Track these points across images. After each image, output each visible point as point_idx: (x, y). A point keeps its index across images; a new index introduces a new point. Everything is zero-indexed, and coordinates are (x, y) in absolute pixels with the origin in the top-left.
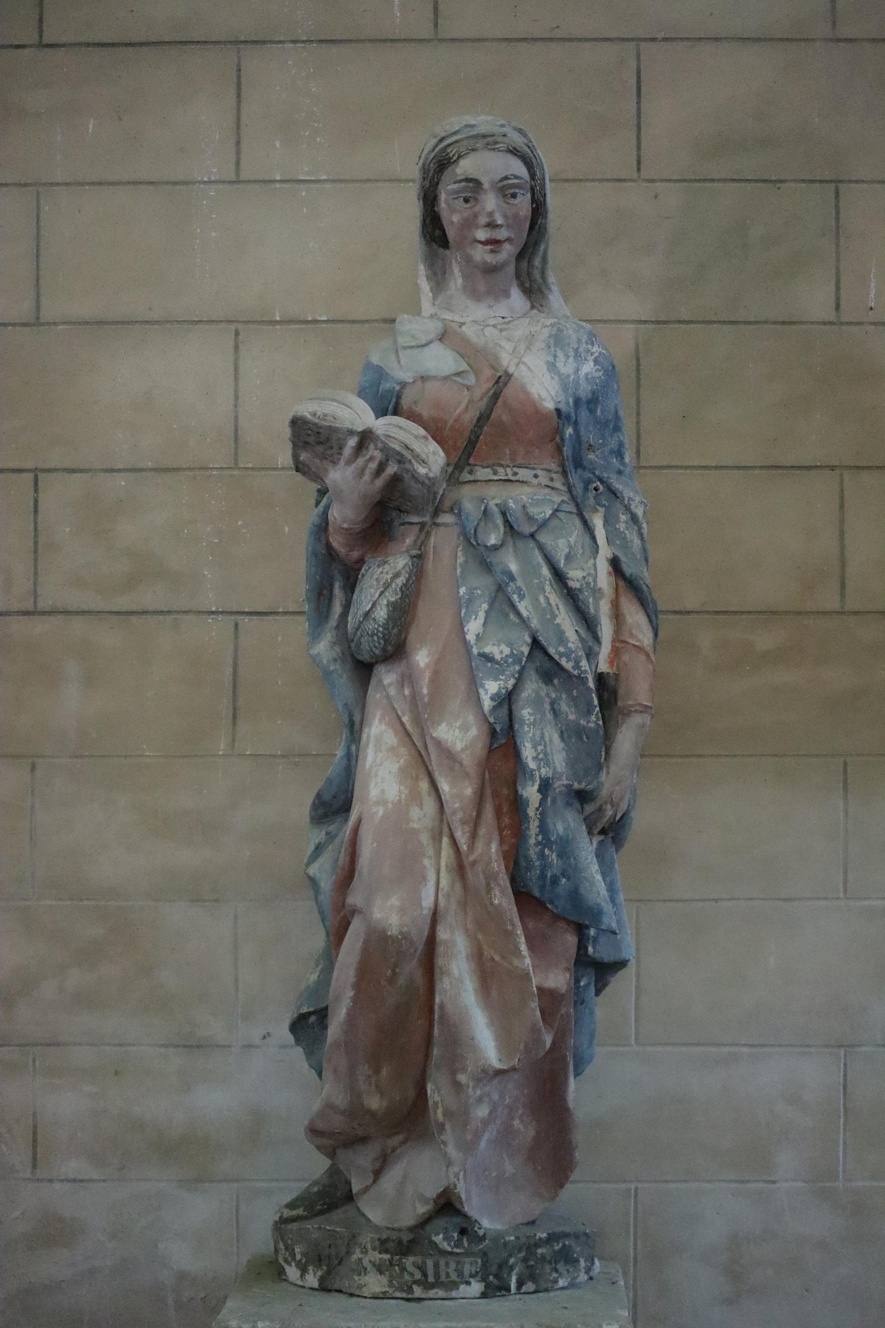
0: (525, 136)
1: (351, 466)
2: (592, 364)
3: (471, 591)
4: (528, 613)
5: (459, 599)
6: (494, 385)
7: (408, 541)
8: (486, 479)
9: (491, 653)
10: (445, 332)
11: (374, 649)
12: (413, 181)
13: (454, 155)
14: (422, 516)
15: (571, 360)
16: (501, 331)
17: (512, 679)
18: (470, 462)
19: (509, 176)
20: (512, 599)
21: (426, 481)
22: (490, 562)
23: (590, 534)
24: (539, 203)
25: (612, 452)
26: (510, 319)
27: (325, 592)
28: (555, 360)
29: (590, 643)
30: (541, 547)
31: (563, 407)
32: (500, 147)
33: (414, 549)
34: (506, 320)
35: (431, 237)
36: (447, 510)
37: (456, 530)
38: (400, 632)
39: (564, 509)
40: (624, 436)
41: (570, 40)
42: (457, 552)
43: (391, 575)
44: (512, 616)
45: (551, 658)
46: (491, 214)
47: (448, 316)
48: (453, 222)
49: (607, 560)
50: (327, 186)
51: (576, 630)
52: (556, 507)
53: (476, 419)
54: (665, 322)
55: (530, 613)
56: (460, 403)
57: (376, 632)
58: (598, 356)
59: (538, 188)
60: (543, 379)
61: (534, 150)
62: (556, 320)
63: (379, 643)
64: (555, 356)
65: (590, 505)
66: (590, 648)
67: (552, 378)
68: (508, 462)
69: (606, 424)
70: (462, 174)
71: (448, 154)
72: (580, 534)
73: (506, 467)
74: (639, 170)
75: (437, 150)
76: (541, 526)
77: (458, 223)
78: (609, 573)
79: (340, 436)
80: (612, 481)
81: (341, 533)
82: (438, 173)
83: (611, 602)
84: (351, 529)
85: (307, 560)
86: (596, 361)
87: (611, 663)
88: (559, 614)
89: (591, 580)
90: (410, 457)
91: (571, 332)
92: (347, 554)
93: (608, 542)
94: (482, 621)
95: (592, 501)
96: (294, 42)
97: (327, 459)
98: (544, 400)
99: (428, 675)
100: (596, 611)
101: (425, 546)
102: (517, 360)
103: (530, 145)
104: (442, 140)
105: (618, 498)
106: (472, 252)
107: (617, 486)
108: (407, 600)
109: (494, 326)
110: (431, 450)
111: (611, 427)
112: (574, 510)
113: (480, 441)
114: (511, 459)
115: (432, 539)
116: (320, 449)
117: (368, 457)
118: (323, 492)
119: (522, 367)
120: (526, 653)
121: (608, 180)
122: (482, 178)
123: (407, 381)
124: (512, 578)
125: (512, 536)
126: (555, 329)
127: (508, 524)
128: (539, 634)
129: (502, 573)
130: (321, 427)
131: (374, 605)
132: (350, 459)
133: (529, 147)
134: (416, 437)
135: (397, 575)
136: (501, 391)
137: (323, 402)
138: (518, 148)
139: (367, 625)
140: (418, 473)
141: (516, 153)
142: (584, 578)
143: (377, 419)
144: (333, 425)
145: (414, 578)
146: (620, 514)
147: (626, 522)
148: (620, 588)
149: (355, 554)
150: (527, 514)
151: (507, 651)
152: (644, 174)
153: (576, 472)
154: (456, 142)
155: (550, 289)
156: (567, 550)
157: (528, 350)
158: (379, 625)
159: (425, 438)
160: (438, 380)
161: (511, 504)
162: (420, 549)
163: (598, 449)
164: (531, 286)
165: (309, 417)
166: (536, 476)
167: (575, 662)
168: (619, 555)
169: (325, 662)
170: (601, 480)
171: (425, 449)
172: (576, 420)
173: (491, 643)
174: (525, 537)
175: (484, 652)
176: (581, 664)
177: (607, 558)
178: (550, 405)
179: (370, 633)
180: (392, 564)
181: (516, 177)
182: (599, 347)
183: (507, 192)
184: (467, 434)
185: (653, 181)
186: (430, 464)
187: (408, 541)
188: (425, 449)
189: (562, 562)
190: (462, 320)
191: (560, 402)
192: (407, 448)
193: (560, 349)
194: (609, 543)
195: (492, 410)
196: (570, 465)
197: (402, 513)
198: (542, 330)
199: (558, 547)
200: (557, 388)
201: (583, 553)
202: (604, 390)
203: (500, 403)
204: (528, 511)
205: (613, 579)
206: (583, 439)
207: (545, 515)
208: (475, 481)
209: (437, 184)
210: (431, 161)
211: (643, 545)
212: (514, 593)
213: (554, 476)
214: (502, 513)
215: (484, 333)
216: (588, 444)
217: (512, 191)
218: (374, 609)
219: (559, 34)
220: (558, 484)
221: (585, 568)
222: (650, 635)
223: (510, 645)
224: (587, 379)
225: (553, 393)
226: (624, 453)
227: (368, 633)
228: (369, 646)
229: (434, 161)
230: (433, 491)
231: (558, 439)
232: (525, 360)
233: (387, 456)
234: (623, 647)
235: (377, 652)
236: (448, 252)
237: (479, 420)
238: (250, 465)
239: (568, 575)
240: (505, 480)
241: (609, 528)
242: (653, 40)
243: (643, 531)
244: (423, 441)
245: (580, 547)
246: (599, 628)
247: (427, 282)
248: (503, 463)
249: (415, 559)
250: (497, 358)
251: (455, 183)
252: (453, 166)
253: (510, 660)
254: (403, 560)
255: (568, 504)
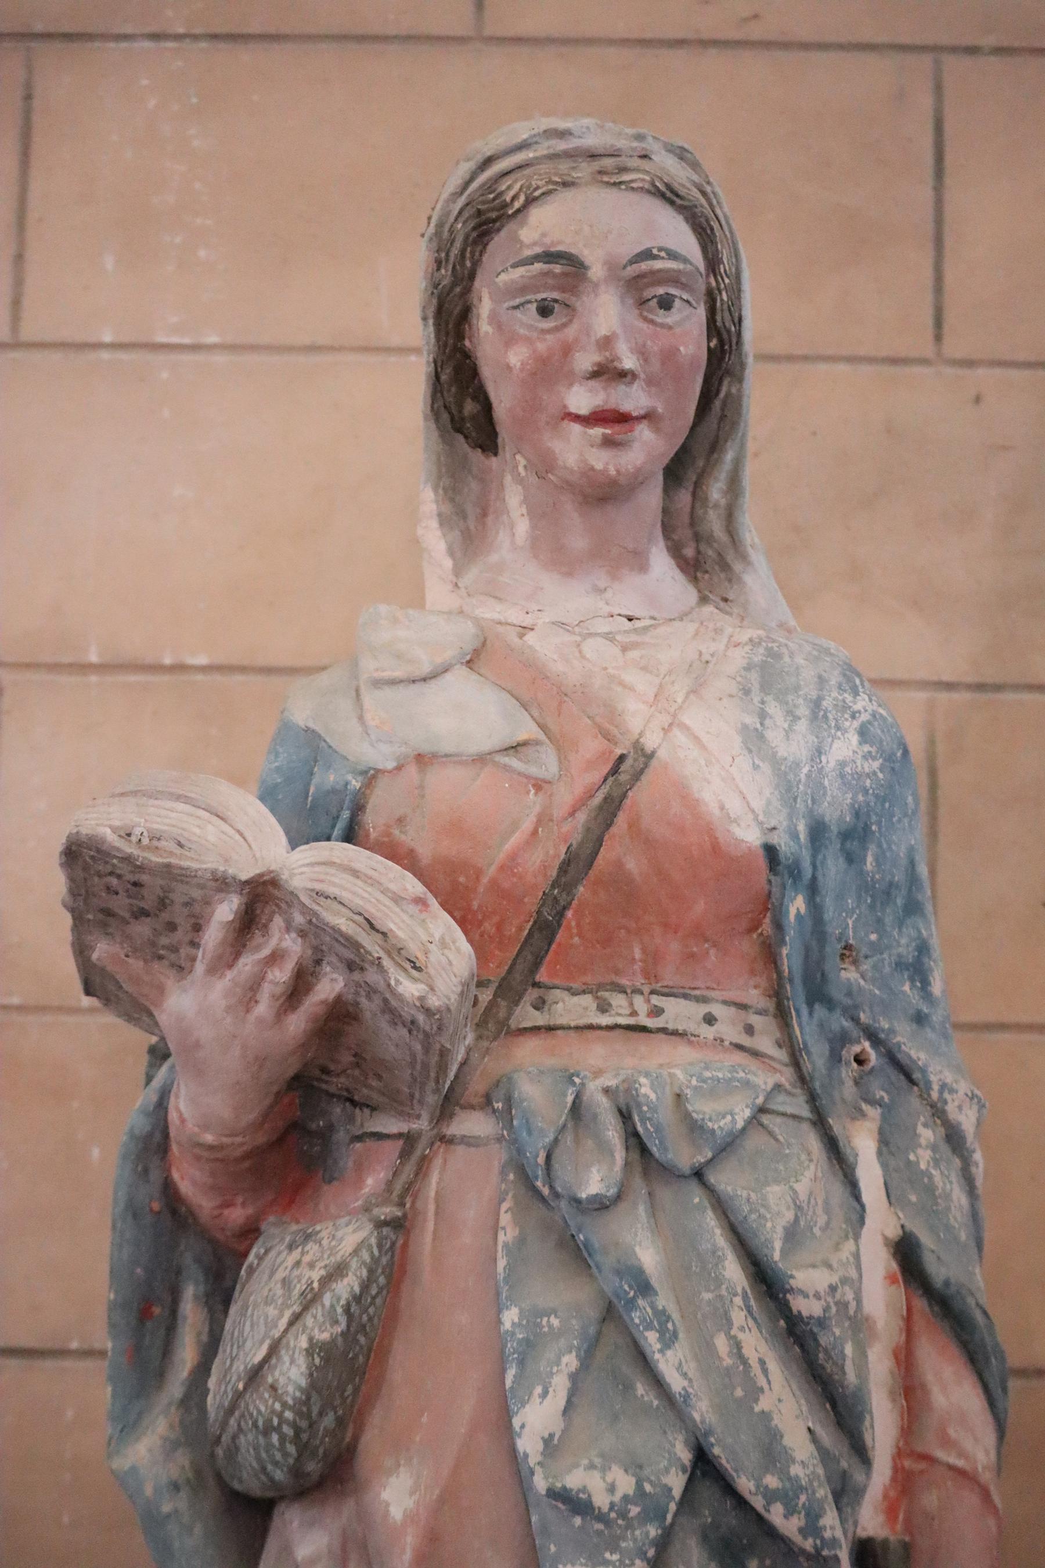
0: (695, 165)
1: (222, 976)
2: (855, 739)
3: (533, 1317)
4: (686, 1383)
5: (501, 1339)
6: (605, 780)
7: (370, 1181)
8: (582, 1022)
9: (584, 1490)
10: (484, 644)
11: (270, 1467)
12: (417, 351)
13: (514, 198)
14: (409, 1115)
15: (802, 726)
16: (625, 649)
17: (638, 1562)
18: (538, 978)
19: (655, 251)
20: (642, 1342)
21: (421, 1018)
22: (587, 1244)
23: (845, 1175)
24: (725, 336)
25: (900, 965)
26: (648, 622)
27: (157, 1310)
28: (762, 724)
29: (844, 1464)
30: (721, 1206)
31: (782, 841)
32: (632, 181)
33: (385, 1202)
34: (637, 624)
35: (452, 420)
36: (475, 1101)
37: (499, 1155)
38: (341, 1422)
39: (781, 1108)
40: (928, 928)
41: (786, 46)
42: (498, 1215)
43: (323, 1272)
44: (640, 1389)
45: (741, 1502)
46: (606, 343)
47: (490, 611)
48: (509, 368)
49: (886, 1245)
50: (220, 359)
51: (809, 1429)
52: (760, 1100)
53: (557, 863)
54: (998, 688)
55: (690, 1380)
56: (515, 826)
57: (275, 1421)
58: (869, 722)
59: (725, 298)
60: (733, 770)
61: (715, 202)
62: (761, 632)
63: (285, 1455)
64: (763, 715)
65: (843, 1100)
66: (844, 1476)
67: (756, 767)
68: (639, 981)
69: (888, 892)
70: (535, 244)
71: (501, 193)
72: (820, 1174)
73: (633, 992)
74: (938, 338)
75: (475, 185)
76: (723, 1150)
77: (522, 370)
78: (892, 1279)
79: (196, 894)
80: (899, 1039)
81: (198, 1158)
82: (475, 242)
83: (896, 1355)
84: (221, 1147)
85: (114, 1227)
86: (863, 733)
87: (891, 1511)
88: (766, 1387)
89: (850, 1296)
90: (377, 951)
91: (800, 660)
92: (216, 1213)
93: (888, 1196)
94: (562, 1403)
95: (849, 1090)
96: (155, 37)
97: (161, 958)
98: (735, 821)
99: (411, 1541)
100: (859, 1376)
101: (415, 1197)
102: (666, 720)
103: (708, 189)
104: (488, 161)
105: (912, 1082)
106: (557, 446)
107: (913, 1054)
108: (362, 1340)
109: (609, 637)
110: (437, 936)
111: (899, 901)
112: (805, 1112)
113: (564, 923)
114: (647, 975)
115: (434, 1178)
116: (142, 929)
117: (266, 952)
118: (159, 1054)
119: (679, 736)
120: (677, 1492)
121: (871, 360)
122: (586, 252)
123: (380, 767)
124: (645, 1288)
125: (646, 1173)
126: (761, 650)
127: (635, 1142)
128: (712, 1440)
129: (618, 1273)
130: (141, 869)
131: (274, 1350)
132: (220, 957)
133: (704, 193)
134: (397, 899)
135: (338, 1271)
136: (624, 795)
137: (152, 802)
138: (676, 186)
139: (254, 1401)
140: (399, 997)
141: (675, 198)
142: (833, 1289)
143: (293, 849)
144: (173, 861)
145: (382, 1280)
146: (919, 1124)
147: (934, 1148)
148: (916, 1317)
149: (237, 1215)
150: (687, 1116)
151: (626, 1484)
152: (955, 346)
153: (811, 1014)
154: (520, 167)
155: (744, 557)
156: (790, 1216)
157: (692, 696)
158: (284, 1405)
159: (419, 901)
160: (461, 763)
161: (646, 1089)
162: (401, 1204)
163: (866, 957)
164: (699, 552)
165: (111, 838)
166: (710, 1020)
167: (807, 1515)
168: (915, 1230)
169: (149, 1491)
170: (873, 1036)
171: (421, 932)
172: (814, 879)
173: (585, 1462)
174: (682, 1176)
175: (564, 1488)
176: (822, 1522)
177: (886, 1238)
178: (750, 836)
179: (260, 1423)
180: (325, 1242)
181: (672, 255)
182: (871, 700)
183: (648, 293)
184: (532, 903)
185: (969, 363)
186: (432, 971)
187: (372, 1182)
188: (421, 932)
189: (778, 1245)
190: (527, 621)
191: (774, 828)
192: (372, 926)
193: (776, 699)
194: (893, 1200)
195: (599, 842)
196: (796, 995)
197: (357, 1111)
198: (729, 653)
199: (766, 1207)
200: (767, 792)
201: (827, 1226)
202: (883, 805)
203: (621, 820)
204: (690, 1108)
205: (899, 1292)
206: (829, 929)
207: (734, 1121)
208: (551, 1029)
209: (472, 276)
210: (456, 220)
211: (972, 1206)
212: (649, 1327)
213: (755, 1020)
214: (620, 1111)
215: (580, 652)
216: (843, 944)
217: (661, 291)
218: (274, 1361)
219: (755, 31)
220: (766, 1043)
221: (835, 1265)
222: (989, 1437)
223: (635, 1466)
224: (842, 776)
225: (758, 804)
226: (931, 970)
227: (255, 1424)
228: (258, 1459)
229: (466, 214)
230: (438, 1046)
231: (767, 927)
232: (686, 719)
233: (317, 949)
234: (922, 1472)
235: (279, 1475)
236: (494, 462)
237: (564, 867)
238: (15, 1000)
239: (792, 1281)
240: (629, 1028)
241: (892, 1163)
242: (972, 50)
243: (973, 1169)
244: (413, 909)
245: (820, 1210)
246: (867, 1423)
247: (439, 533)
248: (624, 982)
249: (385, 1231)
250: (613, 714)
251: (515, 266)
252: (511, 226)
253: (634, 1510)
254: (354, 1231)
255: (789, 1093)
